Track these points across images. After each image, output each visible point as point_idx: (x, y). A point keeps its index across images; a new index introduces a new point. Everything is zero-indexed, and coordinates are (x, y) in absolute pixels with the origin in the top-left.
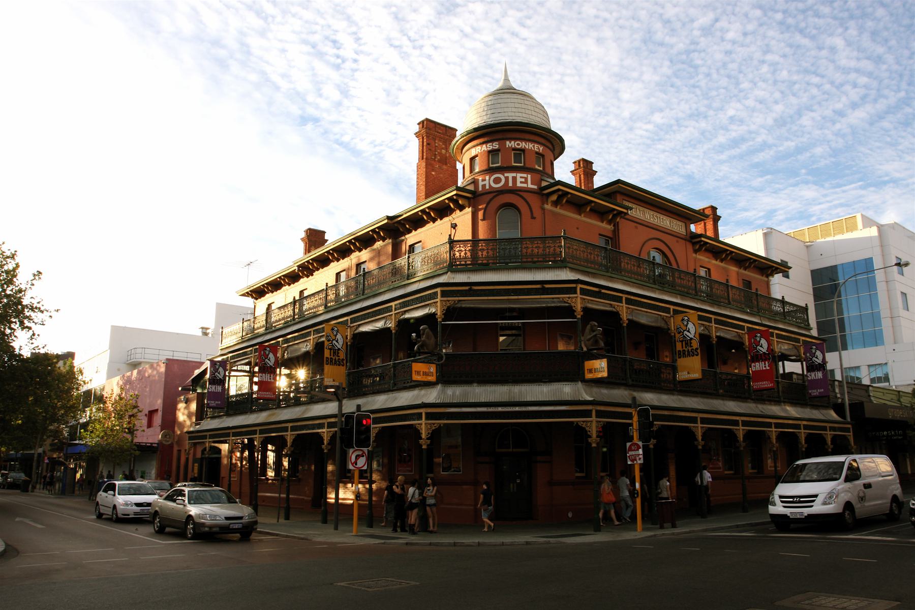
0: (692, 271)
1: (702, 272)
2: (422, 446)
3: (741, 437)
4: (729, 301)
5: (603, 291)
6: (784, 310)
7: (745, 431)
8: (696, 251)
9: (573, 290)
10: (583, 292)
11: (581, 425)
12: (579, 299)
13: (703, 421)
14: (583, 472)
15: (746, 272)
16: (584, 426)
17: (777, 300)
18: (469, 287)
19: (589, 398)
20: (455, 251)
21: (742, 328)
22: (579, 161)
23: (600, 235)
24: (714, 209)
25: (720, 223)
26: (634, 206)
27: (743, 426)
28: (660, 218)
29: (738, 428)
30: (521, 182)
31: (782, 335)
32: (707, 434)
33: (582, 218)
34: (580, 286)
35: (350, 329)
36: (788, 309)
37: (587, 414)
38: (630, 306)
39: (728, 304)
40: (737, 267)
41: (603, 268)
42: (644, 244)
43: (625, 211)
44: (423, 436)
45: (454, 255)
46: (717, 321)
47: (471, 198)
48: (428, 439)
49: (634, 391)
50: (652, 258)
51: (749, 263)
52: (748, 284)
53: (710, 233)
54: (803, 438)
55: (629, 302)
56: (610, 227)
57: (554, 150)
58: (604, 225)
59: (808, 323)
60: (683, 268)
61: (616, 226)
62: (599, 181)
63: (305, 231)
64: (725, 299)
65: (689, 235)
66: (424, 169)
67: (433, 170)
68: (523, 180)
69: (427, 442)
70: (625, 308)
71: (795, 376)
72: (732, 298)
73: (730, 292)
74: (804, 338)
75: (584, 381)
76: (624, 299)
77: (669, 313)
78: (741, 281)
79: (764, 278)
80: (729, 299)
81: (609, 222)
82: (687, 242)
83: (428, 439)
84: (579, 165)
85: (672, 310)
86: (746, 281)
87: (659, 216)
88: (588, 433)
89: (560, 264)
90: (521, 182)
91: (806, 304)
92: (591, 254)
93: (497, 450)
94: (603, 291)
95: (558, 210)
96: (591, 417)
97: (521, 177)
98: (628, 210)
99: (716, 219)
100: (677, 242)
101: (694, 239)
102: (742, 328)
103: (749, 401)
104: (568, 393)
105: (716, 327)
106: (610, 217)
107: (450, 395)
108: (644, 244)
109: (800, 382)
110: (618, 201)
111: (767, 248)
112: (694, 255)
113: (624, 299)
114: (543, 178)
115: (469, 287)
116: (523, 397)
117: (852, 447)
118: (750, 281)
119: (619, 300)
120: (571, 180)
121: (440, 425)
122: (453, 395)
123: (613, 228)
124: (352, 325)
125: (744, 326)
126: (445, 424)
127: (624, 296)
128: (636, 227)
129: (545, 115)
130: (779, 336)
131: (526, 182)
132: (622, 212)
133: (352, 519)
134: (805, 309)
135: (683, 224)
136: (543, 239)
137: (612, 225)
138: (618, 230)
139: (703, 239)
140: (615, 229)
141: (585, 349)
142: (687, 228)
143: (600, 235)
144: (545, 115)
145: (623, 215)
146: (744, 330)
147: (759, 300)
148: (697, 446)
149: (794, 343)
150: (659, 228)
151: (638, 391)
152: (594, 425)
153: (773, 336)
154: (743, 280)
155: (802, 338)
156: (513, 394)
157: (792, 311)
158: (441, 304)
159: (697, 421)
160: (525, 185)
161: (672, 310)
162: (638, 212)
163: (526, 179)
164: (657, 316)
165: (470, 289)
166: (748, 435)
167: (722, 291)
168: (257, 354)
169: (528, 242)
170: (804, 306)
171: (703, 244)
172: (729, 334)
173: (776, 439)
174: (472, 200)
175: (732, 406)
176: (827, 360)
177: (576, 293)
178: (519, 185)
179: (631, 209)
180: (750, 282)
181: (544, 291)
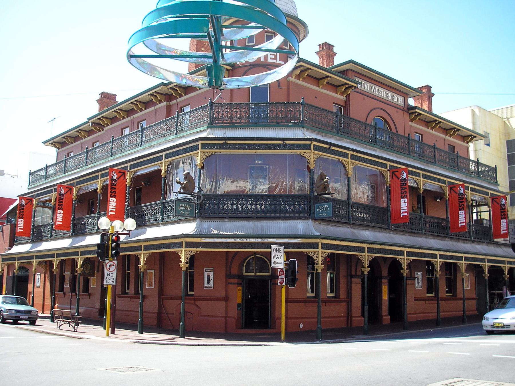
0: (407, 135)
1: (416, 137)
2: (181, 268)
3: (319, 260)
4: (435, 161)
5: (333, 148)
6: (478, 169)
7: (489, 266)
8: (412, 120)
9: (308, 147)
10: (317, 148)
11: (309, 255)
12: (313, 154)
13: (370, 250)
14: (451, 293)
15: (451, 139)
16: (312, 255)
17: (403, 137)
18: (224, 141)
19: (317, 234)
20: (214, 112)
21: (444, 182)
22: (323, 44)
23: (334, 103)
24: (429, 88)
25: (433, 99)
26: (363, 82)
27: (487, 262)
28: (384, 92)
29: (436, 260)
30: (271, 58)
31: (475, 189)
32: (373, 263)
33: (320, 89)
34: (314, 143)
35: (130, 174)
36: (481, 169)
37: (314, 246)
38: (354, 161)
39: (434, 162)
40: (444, 135)
41: (334, 130)
42: (369, 113)
43: (355, 85)
44: (183, 260)
45: (213, 115)
46: (424, 176)
47: (231, 70)
48: (187, 263)
49: (355, 229)
50: (456, 153)
51: (415, 116)
52: (452, 148)
53: (426, 107)
54: (507, 271)
55: (353, 157)
56: (343, 98)
57: (299, 34)
58: (338, 96)
59: (497, 180)
60: (401, 132)
61: (348, 96)
62: (337, 61)
63: (100, 94)
64: (432, 159)
65: (406, 107)
66: (196, 46)
67: (203, 46)
68: (273, 57)
69: (186, 265)
70: (350, 162)
71: (485, 222)
72: (438, 158)
73: (436, 154)
74: (492, 192)
75: (314, 219)
76: (350, 155)
77: (386, 168)
78: (447, 146)
79: (465, 144)
80: (435, 158)
81: (342, 94)
82: (405, 113)
83: (187, 263)
84: (323, 48)
85: (388, 165)
86: (452, 145)
87: (383, 91)
88: (315, 261)
89: (299, 125)
90: (271, 58)
91: (496, 166)
92: (324, 118)
93: (245, 274)
94: (333, 148)
95: (300, 82)
96: (318, 248)
97: (271, 54)
98: (357, 84)
99: (430, 96)
100: (397, 112)
101: (410, 109)
102: (444, 182)
103: (447, 239)
104: (300, 229)
105: (471, 194)
106: (343, 89)
107: (206, 228)
108: (369, 113)
109: (488, 226)
110: (350, 78)
111: (474, 124)
112: (410, 123)
113: (350, 155)
114: (289, 56)
115: (224, 141)
116: (270, 232)
117: (486, 275)
118: (454, 145)
119: (346, 156)
120: (316, 60)
121: (197, 252)
122: (208, 229)
123: (345, 98)
124: (131, 171)
125: (446, 181)
126: (201, 252)
127: (350, 153)
128: (364, 99)
129: (293, 6)
130: (473, 190)
131: (275, 58)
132: (352, 86)
133: (138, 326)
134: (495, 169)
135: (402, 98)
136: (287, 104)
137: (345, 96)
138: (349, 100)
139: (417, 110)
140: (347, 99)
141: (316, 194)
142: (405, 101)
143: (334, 103)
144: (293, 6)
145: (353, 88)
146: (445, 184)
147: (459, 161)
148: (484, 277)
149: (484, 196)
150: (382, 100)
151: (358, 229)
152: (367, 258)
153: (420, 176)
154: (448, 144)
155: (490, 192)
156: (256, 229)
157: (484, 170)
158: (201, 155)
159: (404, 254)
160: (274, 61)
161: (388, 165)
162: (365, 86)
163: (275, 56)
164: (376, 170)
165: (225, 143)
166: (492, 269)
167: (430, 152)
168: (57, 192)
169: (274, 107)
170: (494, 167)
171: (418, 115)
172: (432, 186)
173: (508, 272)
174: (231, 71)
175: (434, 242)
176: (94, 109)
177: (310, 149)
178: (269, 60)
179: (360, 84)
180: (454, 147)
181: (285, 146)
